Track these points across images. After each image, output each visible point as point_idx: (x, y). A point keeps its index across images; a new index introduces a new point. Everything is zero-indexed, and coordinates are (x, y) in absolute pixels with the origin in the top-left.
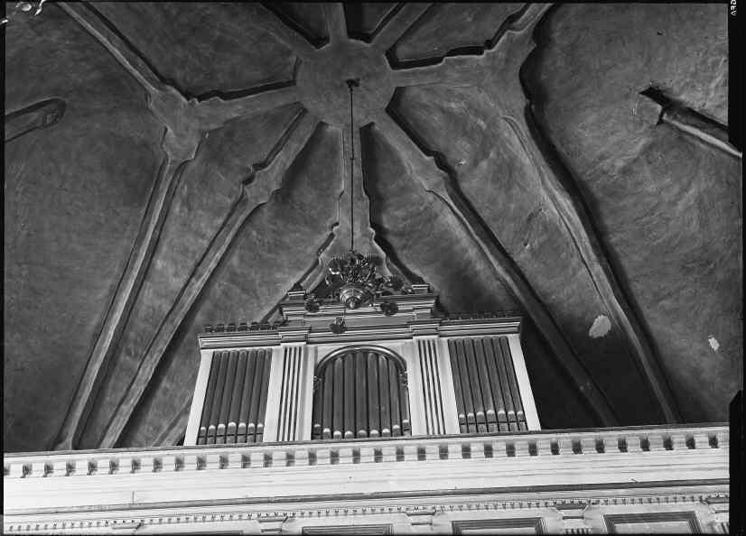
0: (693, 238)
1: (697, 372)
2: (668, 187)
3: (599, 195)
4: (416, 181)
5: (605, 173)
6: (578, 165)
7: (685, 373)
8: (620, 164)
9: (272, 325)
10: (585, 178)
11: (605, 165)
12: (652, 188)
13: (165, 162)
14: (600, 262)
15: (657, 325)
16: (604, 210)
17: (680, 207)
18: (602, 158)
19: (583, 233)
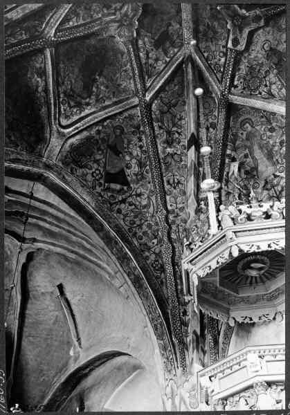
0: (49, 325)
1: (27, 364)
2: (52, 306)
3: (31, 296)
4: (69, 149)
5: (37, 291)
6: (31, 285)
7: (24, 363)
8: (43, 291)
9: (130, 34)
10: (30, 289)
11: (38, 289)
12: (47, 303)
13: (37, 87)
14: (19, 320)
15: (24, 343)
16: (30, 301)
17: (52, 313)
18: (38, 286)
19: (19, 309)
